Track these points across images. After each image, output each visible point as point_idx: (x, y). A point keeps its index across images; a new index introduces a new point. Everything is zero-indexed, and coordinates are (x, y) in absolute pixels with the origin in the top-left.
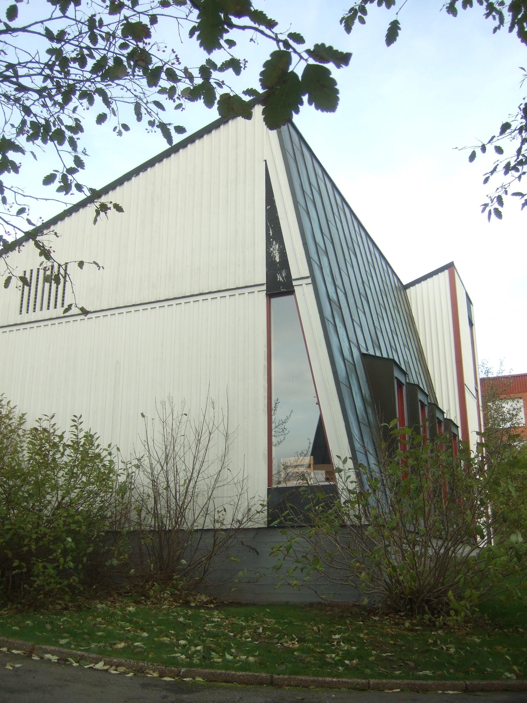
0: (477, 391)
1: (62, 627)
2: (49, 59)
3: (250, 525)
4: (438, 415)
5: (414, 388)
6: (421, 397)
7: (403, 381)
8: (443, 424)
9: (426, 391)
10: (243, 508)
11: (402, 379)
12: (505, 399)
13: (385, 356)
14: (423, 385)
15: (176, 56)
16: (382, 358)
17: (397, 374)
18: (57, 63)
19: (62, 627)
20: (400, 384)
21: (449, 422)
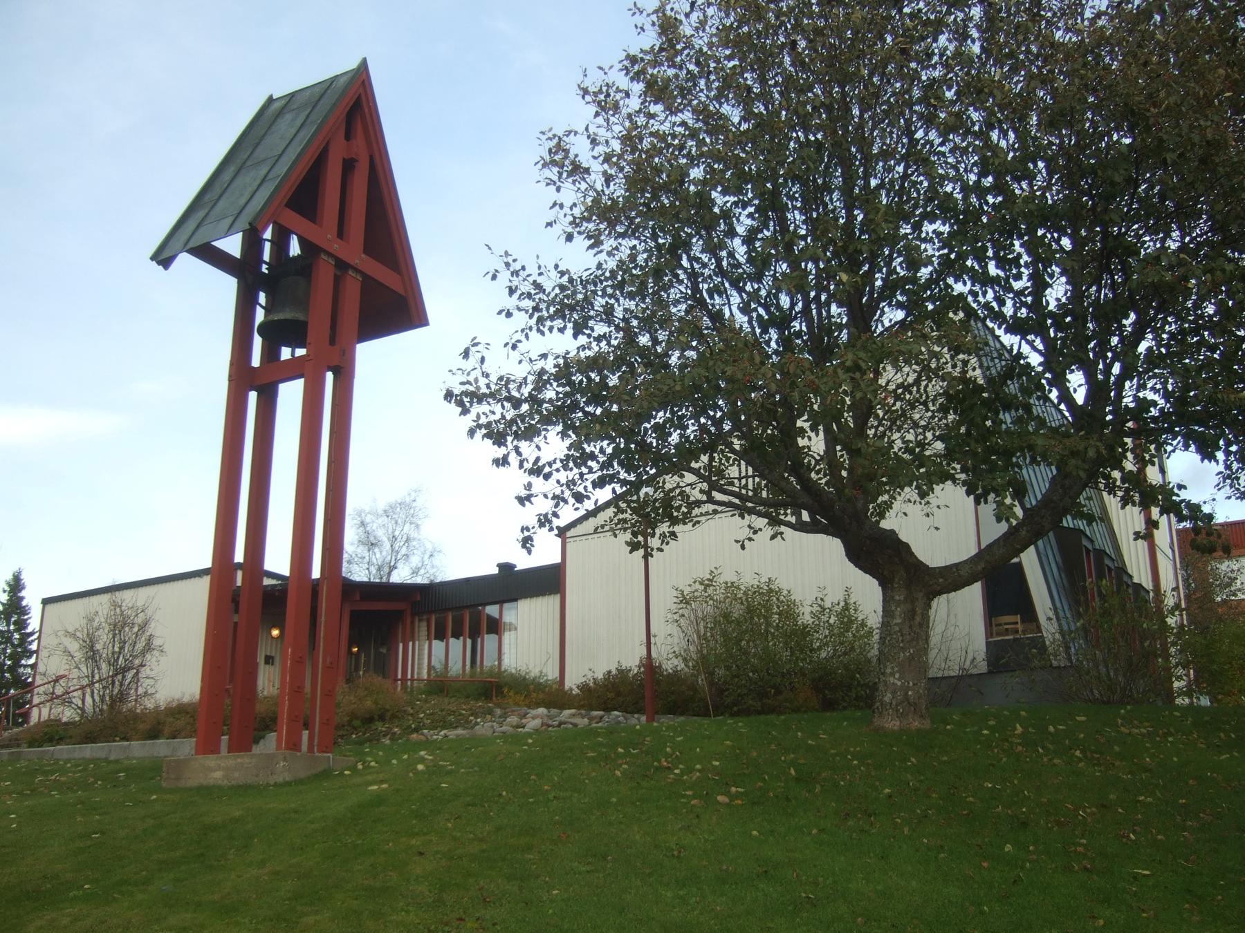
0: (1173, 551)
1: (953, 256)
2: (42, 640)
3: (974, 671)
4: (1125, 578)
5: (1101, 553)
6: (1107, 561)
7: (1090, 548)
8: (1092, 554)
9: (1113, 556)
10: (970, 657)
11: (1090, 547)
12: (1221, 558)
13: (1071, 526)
14: (1109, 550)
15: (761, 530)
16: (1068, 528)
17: (1085, 542)
18: (712, 413)
19: (953, 256)
20: (1088, 551)
21: (1139, 587)
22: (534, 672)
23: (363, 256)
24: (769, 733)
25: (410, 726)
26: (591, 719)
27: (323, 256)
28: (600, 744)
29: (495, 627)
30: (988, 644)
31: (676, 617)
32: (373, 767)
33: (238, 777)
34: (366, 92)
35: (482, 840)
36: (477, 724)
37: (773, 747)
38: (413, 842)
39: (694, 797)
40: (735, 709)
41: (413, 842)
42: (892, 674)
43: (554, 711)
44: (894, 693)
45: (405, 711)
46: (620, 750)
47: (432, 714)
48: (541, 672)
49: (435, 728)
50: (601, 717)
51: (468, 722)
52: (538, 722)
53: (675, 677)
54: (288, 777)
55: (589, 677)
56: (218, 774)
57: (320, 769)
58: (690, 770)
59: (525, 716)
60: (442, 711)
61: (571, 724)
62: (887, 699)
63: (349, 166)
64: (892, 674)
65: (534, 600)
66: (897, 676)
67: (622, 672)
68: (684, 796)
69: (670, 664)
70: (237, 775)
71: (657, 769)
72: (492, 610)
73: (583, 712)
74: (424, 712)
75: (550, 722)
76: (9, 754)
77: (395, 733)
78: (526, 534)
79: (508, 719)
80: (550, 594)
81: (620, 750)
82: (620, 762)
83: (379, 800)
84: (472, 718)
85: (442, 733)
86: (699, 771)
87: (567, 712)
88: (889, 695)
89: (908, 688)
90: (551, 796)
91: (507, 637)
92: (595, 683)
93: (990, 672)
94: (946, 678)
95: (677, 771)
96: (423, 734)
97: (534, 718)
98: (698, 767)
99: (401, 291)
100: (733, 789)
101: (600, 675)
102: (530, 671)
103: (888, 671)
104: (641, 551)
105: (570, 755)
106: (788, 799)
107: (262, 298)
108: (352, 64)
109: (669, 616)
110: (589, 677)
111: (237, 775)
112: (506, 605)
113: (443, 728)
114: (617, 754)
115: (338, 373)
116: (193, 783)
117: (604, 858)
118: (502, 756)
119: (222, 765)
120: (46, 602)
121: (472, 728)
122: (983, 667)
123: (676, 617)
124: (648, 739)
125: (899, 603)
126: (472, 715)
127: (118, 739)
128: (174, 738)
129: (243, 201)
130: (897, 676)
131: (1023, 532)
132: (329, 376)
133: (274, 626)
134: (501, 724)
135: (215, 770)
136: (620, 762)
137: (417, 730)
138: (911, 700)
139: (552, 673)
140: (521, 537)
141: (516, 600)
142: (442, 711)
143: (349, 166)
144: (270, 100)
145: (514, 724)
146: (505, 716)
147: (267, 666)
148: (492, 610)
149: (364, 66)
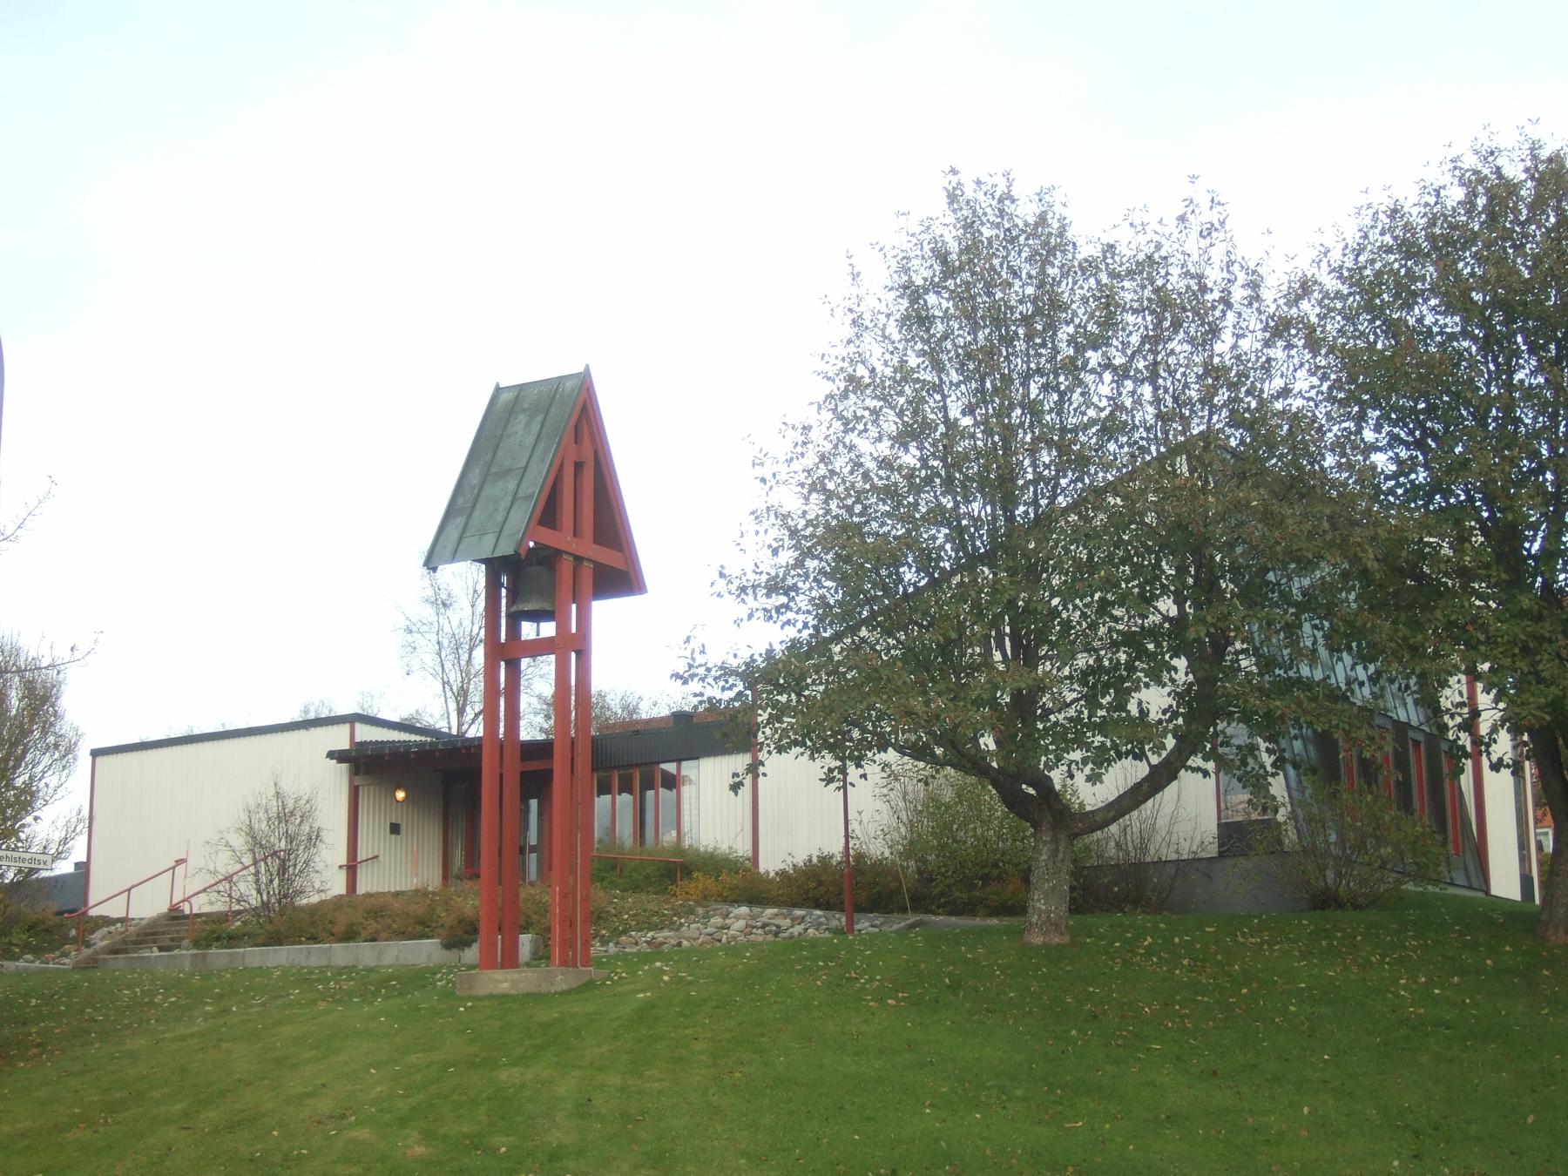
3: (1204, 855)
22: (724, 848)
23: (595, 546)
24: (940, 947)
25: (616, 929)
26: (793, 919)
27: (565, 557)
28: (806, 958)
29: (672, 782)
30: (1219, 825)
31: (885, 791)
32: (625, 978)
33: (523, 988)
34: (590, 398)
35: (731, 1030)
36: (682, 925)
37: (939, 960)
38: (687, 1032)
39: (872, 1000)
40: (942, 900)
41: (687, 1032)
42: (1039, 900)
43: (756, 910)
44: (1040, 915)
45: (608, 912)
46: (821, 964)
47: (635, 915)
48: (730, 848)
49: (641, 930)
50: (803, 917)
51: (673, 923)
52: (741, 924)
53: (880, 867)
54: (565, 987)
55: (789, 862)
56: (506, 985)
57: (585, 980)
58: (871, 980)
59: (726, 916)
60: (645, 911)
61: (776, 926)
62: (1034, 920)
63: (579, 466)
64: (1039, 900)
65: (726, 757)
66: (1042, 902)
67: (825, 860)
68: (866, 1000)
69: (878, 849)
70: (522, 985)
71: (848, 979)
72: (670, 767)
73: (785, 911)
74: (627, 913)
75: (754, 923)
76: (192, 955)
77: (604, 936)
78: (737, 780)
79: (712, 920)
80: (738, 753)
81: (821, 964)
82: (820, 973)
83: (649, 1005)
84: (675, 918)
85: (650, 935)
86: (878, 980)
87: (770, 911)
88: (1036, 917)
89: (1051, 911)
90: (772, 1001)
91: (687, 791)
92: (794, 870)
93: (1221, 855)
94: (1198, 859)
95: (862, 981)
96: (631, 936)
97: (737, 918)
98: (878, 977)
99: (623, 568)
100: (900, 995)
101: (800, 860)
102: (718, 846)
103: (1036, 897)
104: (923, 229)
105: (782, 968)
106: (937, 1001)
107: (504, 579)
108: (581, 369)
109: (877, 791)
110: (789, 862)
111: (522, 985)
112: (685, 764)
113: (650, 929)
114: (818, 966)
115: (578, 653)
116: (484, 991)
117: (810, 1040)
118: (729, 969)
119: (509, 978)
120: (96, 753)
121: (677, 930)
122: (1213, 851)
123: (885, 791)
124: (843, 953)
125: (1045, 843)
126: (675, 915)
127: (303, 939)
128: (374, 940)
129: (499, 518)
130: (1042, 902)
131: (1145, 788)
132: (573, 655)
133: (399, 787)
134: (705, 925)
135: (502, 982)
136: (820, 973)
137: (624, 932)
138: (1053, 921)
139: (743, 848)
140: (731, 781)
141: (697, 758)
142: (645, 911)
143: (579, 466)
144: (498, 391)
145: (719, 925)
146: (707, 916)
147: (394, 836)
148: (670, 767)
149: (587, 369)
